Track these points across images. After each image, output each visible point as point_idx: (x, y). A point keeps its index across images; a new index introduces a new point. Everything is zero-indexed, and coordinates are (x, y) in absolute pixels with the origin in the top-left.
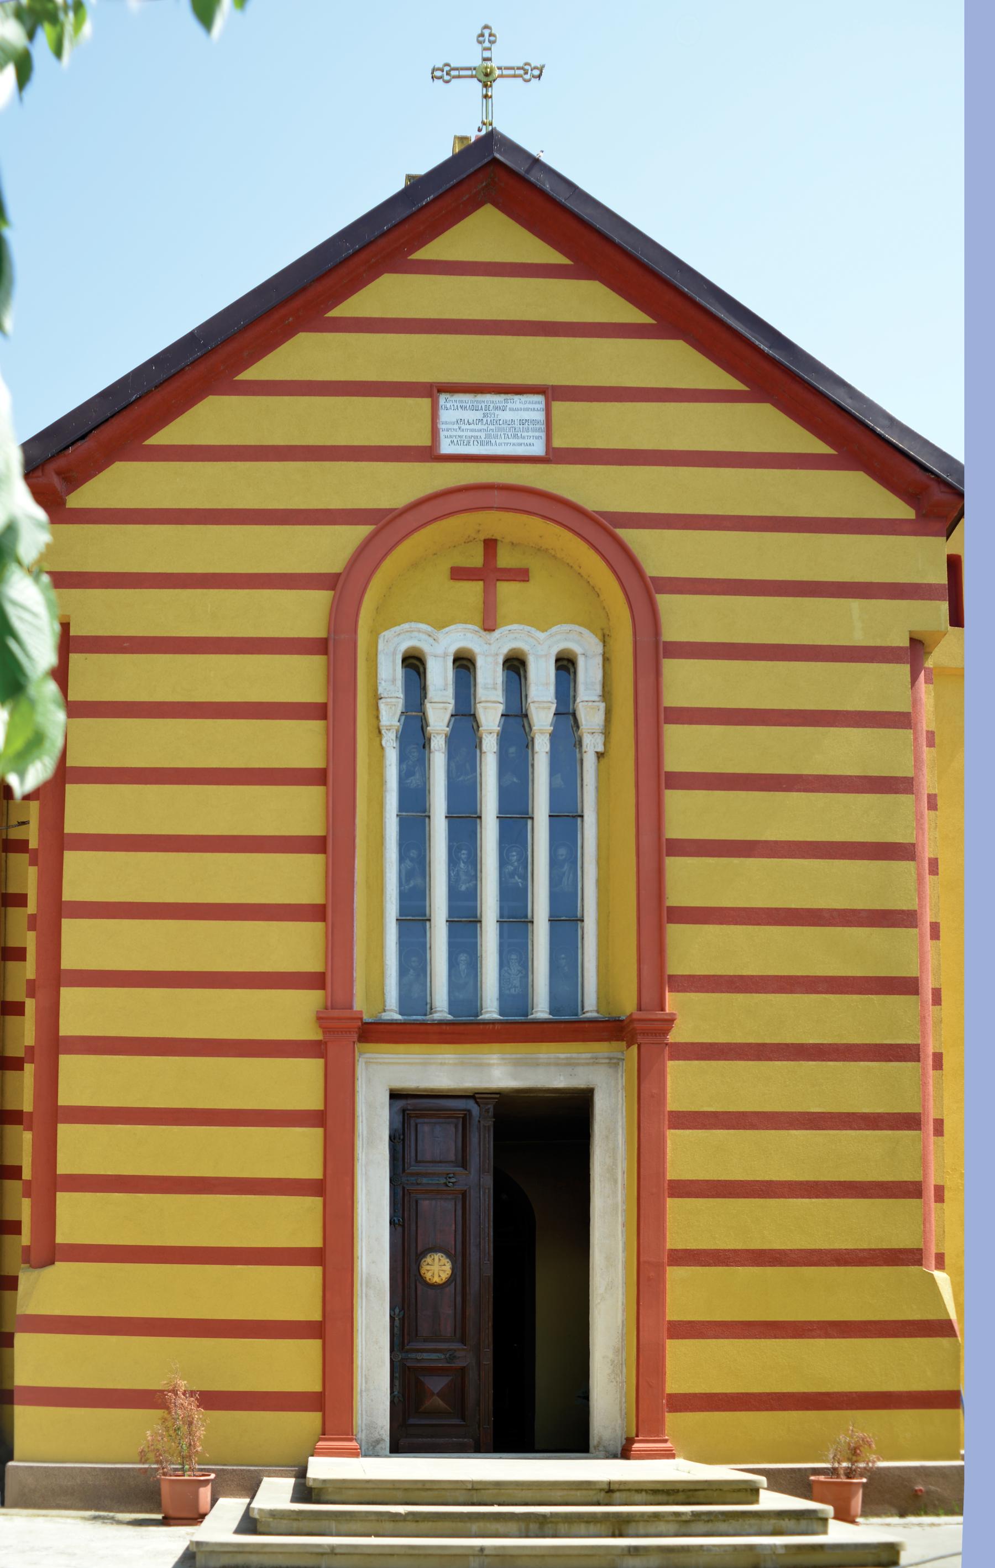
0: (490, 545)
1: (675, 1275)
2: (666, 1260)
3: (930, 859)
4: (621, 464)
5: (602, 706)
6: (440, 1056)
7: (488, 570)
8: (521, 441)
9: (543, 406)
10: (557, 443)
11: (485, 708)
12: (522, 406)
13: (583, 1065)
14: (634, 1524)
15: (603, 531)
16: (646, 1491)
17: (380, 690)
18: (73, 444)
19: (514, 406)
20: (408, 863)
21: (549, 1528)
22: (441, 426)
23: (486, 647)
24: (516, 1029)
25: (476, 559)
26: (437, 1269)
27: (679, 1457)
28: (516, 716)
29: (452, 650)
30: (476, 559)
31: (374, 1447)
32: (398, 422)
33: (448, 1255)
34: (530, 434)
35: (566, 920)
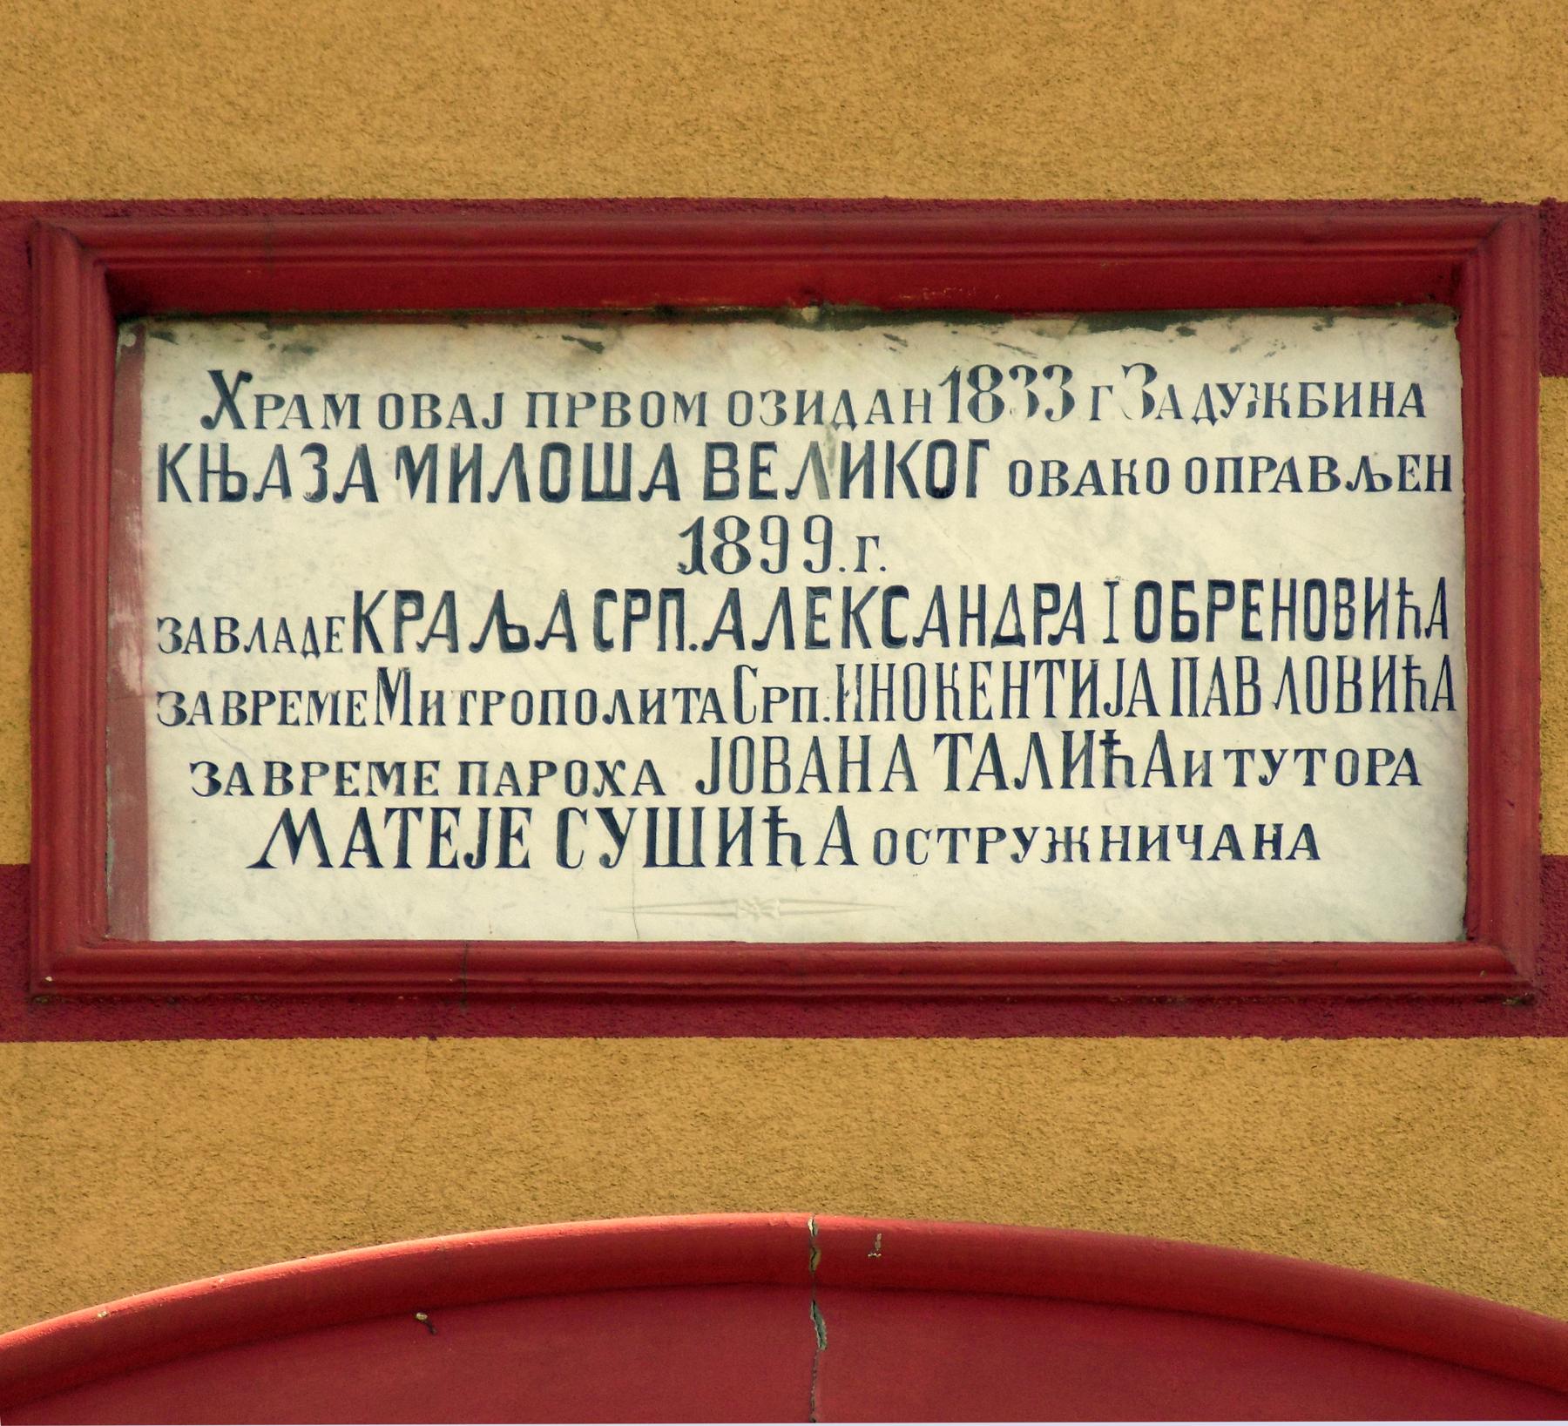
9: (1436, 431)
12: (1177, 442)
19: (1069, 442)
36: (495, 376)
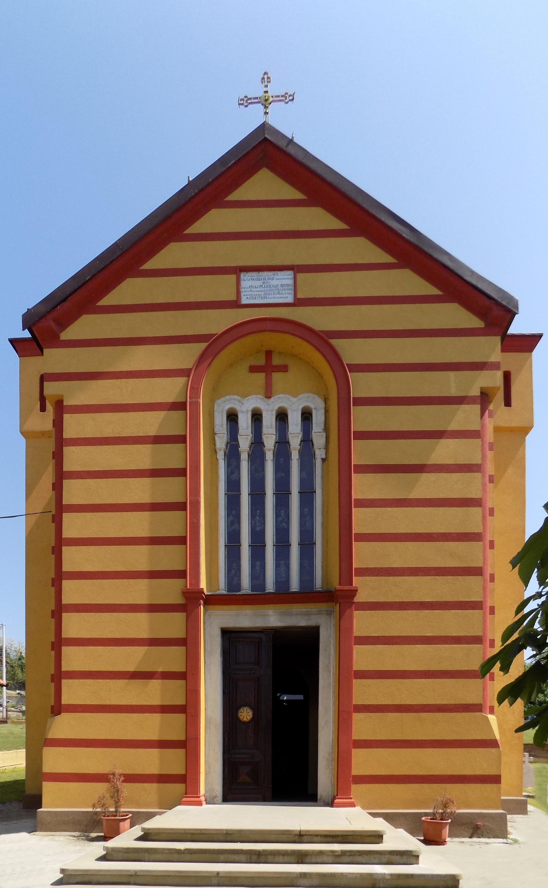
0: (269, 354)
1: (357, 717)
2: (352, 710)
3: (489, 508)
4: (332, 305)
5: (324, 434)
6: (245, 611)
7: (268, 367)
8: (281, 296)
9: (292, 276)
10: (299, 296)
11: (267, 438)
13: (314, 614)
14: (309, 856)
15: (322, 340)
16: (321, 836)
17: (216, 430)
18: (59, 304)
20: (231, 518)
21: (262, 858)
22: (242, 290)
23: (267, 406)
24: (283, 596)
25: (261, 361)
26: (246, 714)
27: (358, 806)
28: (282, 443)
29: (251, 408)
30: (261, 361)
31: (213, 799)
32: (219, 288)
33: (251, 708)
34: (286, 292)
35: (307, 544)
36: (254, 274)
